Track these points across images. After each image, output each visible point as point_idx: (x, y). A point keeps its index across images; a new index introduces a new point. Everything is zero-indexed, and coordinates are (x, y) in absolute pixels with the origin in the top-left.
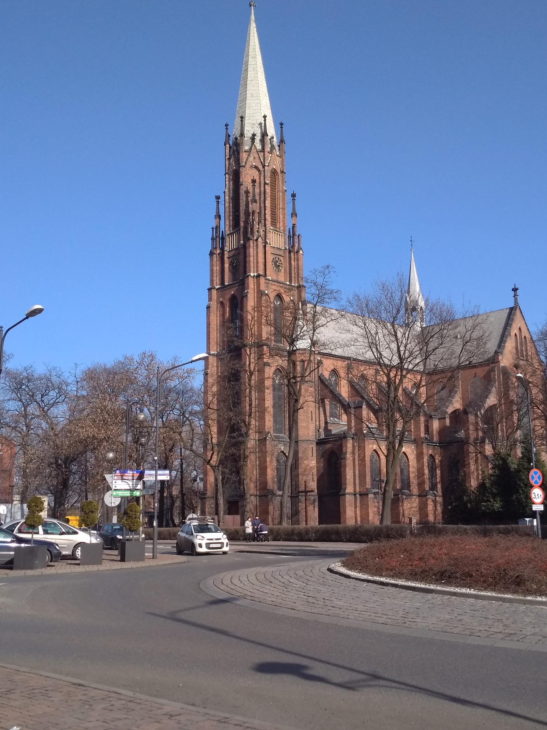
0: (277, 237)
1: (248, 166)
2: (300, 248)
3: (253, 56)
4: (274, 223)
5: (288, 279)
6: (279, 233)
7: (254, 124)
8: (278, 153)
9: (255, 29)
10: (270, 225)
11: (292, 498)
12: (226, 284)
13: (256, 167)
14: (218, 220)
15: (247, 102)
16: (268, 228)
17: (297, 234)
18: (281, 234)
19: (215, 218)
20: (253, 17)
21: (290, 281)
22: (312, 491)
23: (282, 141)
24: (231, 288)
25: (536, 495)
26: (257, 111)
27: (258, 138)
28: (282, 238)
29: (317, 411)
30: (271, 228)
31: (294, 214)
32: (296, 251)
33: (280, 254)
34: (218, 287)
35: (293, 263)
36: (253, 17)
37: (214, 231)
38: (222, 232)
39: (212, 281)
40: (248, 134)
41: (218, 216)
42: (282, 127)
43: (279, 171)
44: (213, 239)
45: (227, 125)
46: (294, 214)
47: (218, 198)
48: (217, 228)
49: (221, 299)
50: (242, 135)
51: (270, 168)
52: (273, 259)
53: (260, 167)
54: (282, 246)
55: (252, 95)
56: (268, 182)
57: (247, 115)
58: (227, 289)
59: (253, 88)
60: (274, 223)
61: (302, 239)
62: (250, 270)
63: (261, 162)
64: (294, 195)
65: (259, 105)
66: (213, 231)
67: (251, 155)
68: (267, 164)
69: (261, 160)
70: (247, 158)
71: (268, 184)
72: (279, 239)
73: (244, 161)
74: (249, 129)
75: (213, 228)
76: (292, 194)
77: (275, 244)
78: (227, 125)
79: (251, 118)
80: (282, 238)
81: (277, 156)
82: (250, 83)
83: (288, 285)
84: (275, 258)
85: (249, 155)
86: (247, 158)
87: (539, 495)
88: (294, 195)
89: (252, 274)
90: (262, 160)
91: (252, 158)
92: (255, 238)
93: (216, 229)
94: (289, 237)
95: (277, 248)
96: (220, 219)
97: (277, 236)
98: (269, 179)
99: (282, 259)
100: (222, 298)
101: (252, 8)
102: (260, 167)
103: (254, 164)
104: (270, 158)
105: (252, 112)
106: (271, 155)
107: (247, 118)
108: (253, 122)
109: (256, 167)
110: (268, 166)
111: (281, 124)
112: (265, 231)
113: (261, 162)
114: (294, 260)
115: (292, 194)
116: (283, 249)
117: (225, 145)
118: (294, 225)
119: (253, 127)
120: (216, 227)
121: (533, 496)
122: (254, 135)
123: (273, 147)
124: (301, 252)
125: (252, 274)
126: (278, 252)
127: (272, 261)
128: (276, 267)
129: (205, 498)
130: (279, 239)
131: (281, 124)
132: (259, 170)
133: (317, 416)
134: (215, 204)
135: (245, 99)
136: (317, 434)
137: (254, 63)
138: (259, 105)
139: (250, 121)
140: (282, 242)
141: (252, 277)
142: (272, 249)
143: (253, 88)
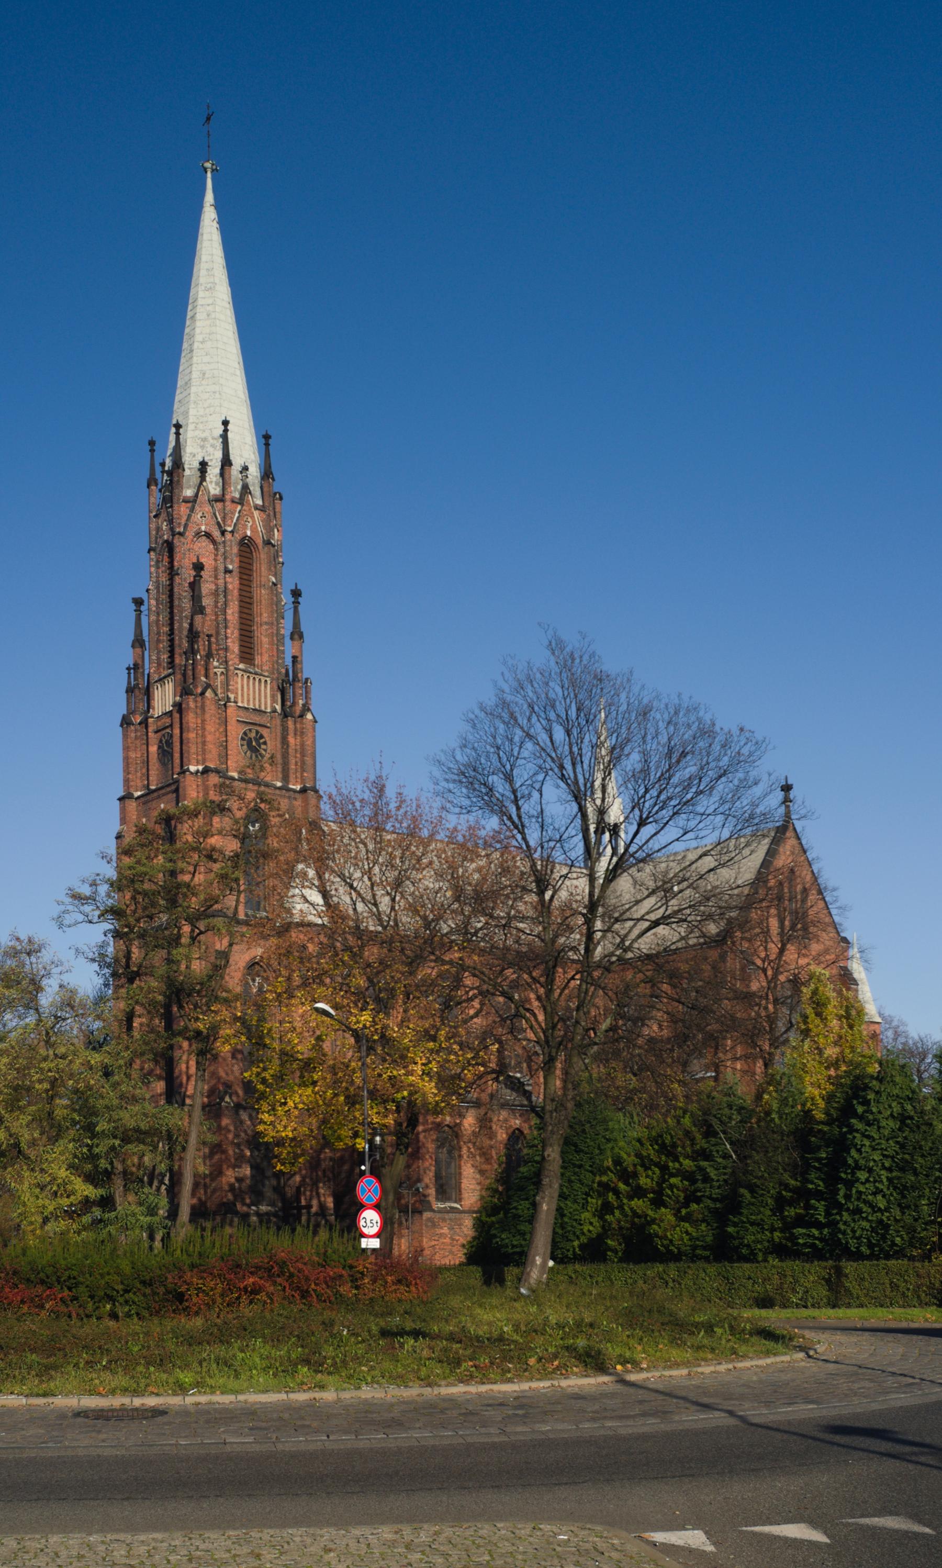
0: (248, 685)
1: (190, 534)
2: (306, 708)
3: (208, 286)
4: (247, 654)
5: (280, 775)
6: (257, 678)
7: (204, 440)
8: (259, 502)
9: (215, 225)
10: (237, 661)
12: (153, 787)
13: (208, 535)
15: (193, 389)
16: (232, 668)
18: (263, 679)
19: (133, 646)
20: (209, 197)
21: (285, 779)
23: (267, 474)
25: (368, 1222)
26: (212, 409)
27: (213, 472)
28: (266, 687)
30: (241, 666)
31: (297, 634)
32: (298, 713)
33: (262, 722)
34: (139, 793)
35: (291, 740)
36: (209, 197)
37: (132, 675)
39: (126, 781)
40: (191, 463)
41: (138, 642)
43: (259, 542)
44: (130, 690)
45: (152, 443)
47: (138, 602)
48: (136, 668)
50: (178, 464)
51: (238, 536)
52: (245, 733)
53: (216, 534)
54: (266, 704)
55: (204, 374)
56: (230, 567)
57: (192, 419)
59: (206, 359)
60: (247, 654)
62: (189, 761)
63: (218, 523)
64: (296, 593)
65: (217, 395)
66: (129, 674)
67: (197, 507)
68: (229, 529)
69: (217, 519)
70: (189, 516)
71: (230, 572)
72: (260, 690)
73: (183, 522)
74: (195, 451)
75: (128, 669)
76: (292, 591)
77: (248, 701)
78: (152, 443)
79: (201, 426)
80: (266, 687)
81: (256, 507)
82: (201, 346)
83: (279, 788)
84: (248, 732)
85: (192, 510)
86: (189, 516)
87: (374, 1222)
88: (296, 593)
89: (193, 768)
90: (219, 520)
91: (199, 516)
92: (199, 690)
95: (255, 710)
97: (248, 682)
98: (236, 560)
99: (265, 732)
100: (145, 816)
102: (216, 534)
103: (203, 528)
104: (237, 515)
105: (201, 412)
106: (239, 507)
107: (191, 427)
108: (203, 435)
109: (208, 535)
110: (232, 532)
111: (267, 437)
112: (226, 674)
113: (218, 523)
114: (295, 734)
115: (292, 591)
117: (148, 487)
119: (202, 447)
121: (362, 1223)
122: (203, 465)
123: (246, 489)
124: (309, 716)
125: (193, 768)
126: (257, 719)
127: (242, 739)
128: (252, 751)
130: (260, 690)
132: (214, 542)
134: (133, 615)
135: (188, 384)
137: (210, 301)
138: (217, 395)
139: (197, 433)
140: (266, 697)
141: (192, 773)
142: (241, 713)
143: (206, 359)
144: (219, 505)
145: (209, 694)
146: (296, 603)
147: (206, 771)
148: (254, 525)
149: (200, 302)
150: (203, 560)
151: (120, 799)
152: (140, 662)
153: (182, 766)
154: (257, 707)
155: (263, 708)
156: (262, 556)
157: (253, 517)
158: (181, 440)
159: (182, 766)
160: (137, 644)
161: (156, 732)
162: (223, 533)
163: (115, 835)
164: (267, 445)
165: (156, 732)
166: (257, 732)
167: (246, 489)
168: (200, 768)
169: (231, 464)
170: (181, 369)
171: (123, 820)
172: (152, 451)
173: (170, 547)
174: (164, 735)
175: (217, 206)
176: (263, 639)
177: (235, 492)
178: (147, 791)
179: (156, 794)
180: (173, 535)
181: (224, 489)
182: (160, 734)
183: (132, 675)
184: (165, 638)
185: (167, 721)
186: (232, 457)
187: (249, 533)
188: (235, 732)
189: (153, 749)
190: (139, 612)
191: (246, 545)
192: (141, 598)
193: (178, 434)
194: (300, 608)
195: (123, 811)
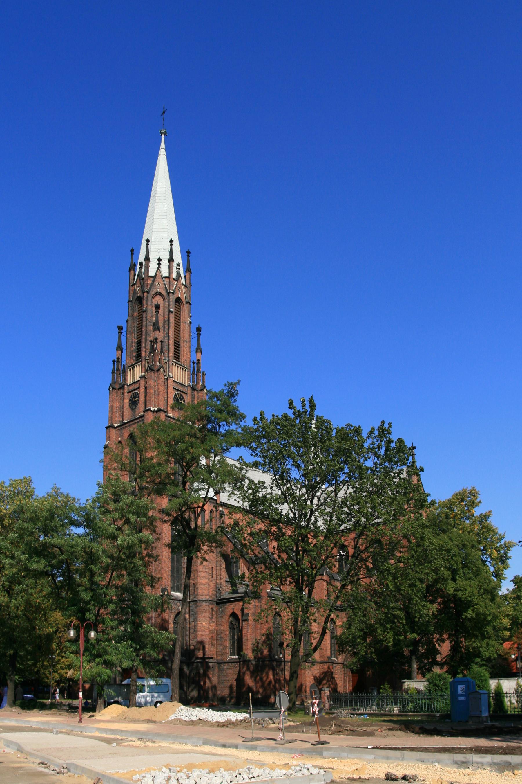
4: (177, 357)
11: (487, 695)
14: (120, 352)
17: (202, 370)
20: (163, 145)
22: (211, 658)
24: (130, 425)
29: (218, 568)
31: (199, 349)
34: (117, 425)
36: (163, 145)
38: (124, 366)
39: (111, 419)
41: (119, 348)
42: (188, 256)
43: (184, 300)
45: (132, 251)
46: (199, 349)
47: (120, 328)
49: (120, 439)
51: (175, 296)
52: (176, 395)
56: (172, 310)
58: (127, 427)
60: (177, 357)
61: (206, 378)
66: (114, 364)
71: (172, 312)
75: (114, 361)
78: (132, 251)
81: (183, 285)
88: (199, 330)
93: (118, 361)
94: (193, 373)
95: (180, 384)
96: (122, 352)
99: (184, 395)
100: (120, 437)
101: (163, 136)
106: (176, 282)
111: (188, 252)
113: (166, 288)
116: (186, 385)
117: (130, 271)
118: (99, 779)
120: (118, 359)
123: (179, 274)
129: (317, 725)
131: (188, 252)
133: (218, 573)
136: (218, 593)
142: (175, 384)
144: (167, 280)
145: (162, 370)
146: (199, 335)
147: (159, 410)
148: (182, 293)
149: (158, 188)
150: (159, 303)
151: (107, 428)
152: (120, 357)
153: (146, 407)
154: (181, 382)
155: (184, 383)
156: (185, 308)
157: (181, 289)
158: (149, 248)
159: (146, 407)
160: (119, 349)
161: (128, 393)
162: (169, 293)
163: (103, 446)
164: (188, 256)
165: (128, 393)
166: (181, 395)
167: (179, 274)
168: (156, 409)
169: (173, 261)
170: (147, 218)
171: (108, 438)
172: (132, 254)
173: (140, 300)
174: (133, 394)
175: (166, 149)
176: (184, 349)
177: (174, 276)
178: (122, 423)
179: (128, 424)
180: (143, 293)
181: (169, 274)
182: (131, 394)
183: (115, 365)
184: (135, 345)
185: (136, 386)
186: (174, 258)
187: (180, 296)
188: (172, 393)
189: (127, 401)
190: (120, 333)
191: (178, 300)
192: (122, 326)
193: (147, 244)
194: (201, 337)
195: (108, 433)
